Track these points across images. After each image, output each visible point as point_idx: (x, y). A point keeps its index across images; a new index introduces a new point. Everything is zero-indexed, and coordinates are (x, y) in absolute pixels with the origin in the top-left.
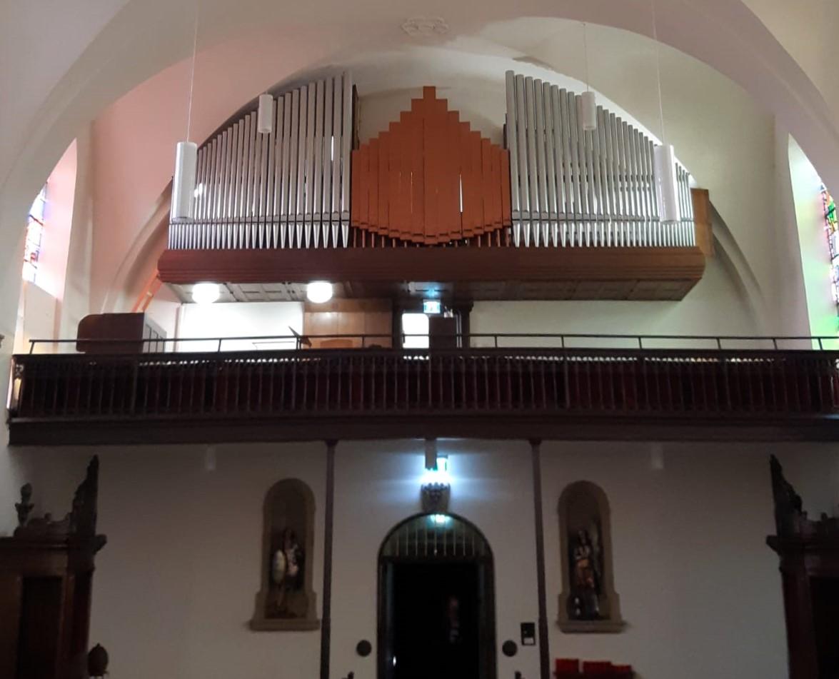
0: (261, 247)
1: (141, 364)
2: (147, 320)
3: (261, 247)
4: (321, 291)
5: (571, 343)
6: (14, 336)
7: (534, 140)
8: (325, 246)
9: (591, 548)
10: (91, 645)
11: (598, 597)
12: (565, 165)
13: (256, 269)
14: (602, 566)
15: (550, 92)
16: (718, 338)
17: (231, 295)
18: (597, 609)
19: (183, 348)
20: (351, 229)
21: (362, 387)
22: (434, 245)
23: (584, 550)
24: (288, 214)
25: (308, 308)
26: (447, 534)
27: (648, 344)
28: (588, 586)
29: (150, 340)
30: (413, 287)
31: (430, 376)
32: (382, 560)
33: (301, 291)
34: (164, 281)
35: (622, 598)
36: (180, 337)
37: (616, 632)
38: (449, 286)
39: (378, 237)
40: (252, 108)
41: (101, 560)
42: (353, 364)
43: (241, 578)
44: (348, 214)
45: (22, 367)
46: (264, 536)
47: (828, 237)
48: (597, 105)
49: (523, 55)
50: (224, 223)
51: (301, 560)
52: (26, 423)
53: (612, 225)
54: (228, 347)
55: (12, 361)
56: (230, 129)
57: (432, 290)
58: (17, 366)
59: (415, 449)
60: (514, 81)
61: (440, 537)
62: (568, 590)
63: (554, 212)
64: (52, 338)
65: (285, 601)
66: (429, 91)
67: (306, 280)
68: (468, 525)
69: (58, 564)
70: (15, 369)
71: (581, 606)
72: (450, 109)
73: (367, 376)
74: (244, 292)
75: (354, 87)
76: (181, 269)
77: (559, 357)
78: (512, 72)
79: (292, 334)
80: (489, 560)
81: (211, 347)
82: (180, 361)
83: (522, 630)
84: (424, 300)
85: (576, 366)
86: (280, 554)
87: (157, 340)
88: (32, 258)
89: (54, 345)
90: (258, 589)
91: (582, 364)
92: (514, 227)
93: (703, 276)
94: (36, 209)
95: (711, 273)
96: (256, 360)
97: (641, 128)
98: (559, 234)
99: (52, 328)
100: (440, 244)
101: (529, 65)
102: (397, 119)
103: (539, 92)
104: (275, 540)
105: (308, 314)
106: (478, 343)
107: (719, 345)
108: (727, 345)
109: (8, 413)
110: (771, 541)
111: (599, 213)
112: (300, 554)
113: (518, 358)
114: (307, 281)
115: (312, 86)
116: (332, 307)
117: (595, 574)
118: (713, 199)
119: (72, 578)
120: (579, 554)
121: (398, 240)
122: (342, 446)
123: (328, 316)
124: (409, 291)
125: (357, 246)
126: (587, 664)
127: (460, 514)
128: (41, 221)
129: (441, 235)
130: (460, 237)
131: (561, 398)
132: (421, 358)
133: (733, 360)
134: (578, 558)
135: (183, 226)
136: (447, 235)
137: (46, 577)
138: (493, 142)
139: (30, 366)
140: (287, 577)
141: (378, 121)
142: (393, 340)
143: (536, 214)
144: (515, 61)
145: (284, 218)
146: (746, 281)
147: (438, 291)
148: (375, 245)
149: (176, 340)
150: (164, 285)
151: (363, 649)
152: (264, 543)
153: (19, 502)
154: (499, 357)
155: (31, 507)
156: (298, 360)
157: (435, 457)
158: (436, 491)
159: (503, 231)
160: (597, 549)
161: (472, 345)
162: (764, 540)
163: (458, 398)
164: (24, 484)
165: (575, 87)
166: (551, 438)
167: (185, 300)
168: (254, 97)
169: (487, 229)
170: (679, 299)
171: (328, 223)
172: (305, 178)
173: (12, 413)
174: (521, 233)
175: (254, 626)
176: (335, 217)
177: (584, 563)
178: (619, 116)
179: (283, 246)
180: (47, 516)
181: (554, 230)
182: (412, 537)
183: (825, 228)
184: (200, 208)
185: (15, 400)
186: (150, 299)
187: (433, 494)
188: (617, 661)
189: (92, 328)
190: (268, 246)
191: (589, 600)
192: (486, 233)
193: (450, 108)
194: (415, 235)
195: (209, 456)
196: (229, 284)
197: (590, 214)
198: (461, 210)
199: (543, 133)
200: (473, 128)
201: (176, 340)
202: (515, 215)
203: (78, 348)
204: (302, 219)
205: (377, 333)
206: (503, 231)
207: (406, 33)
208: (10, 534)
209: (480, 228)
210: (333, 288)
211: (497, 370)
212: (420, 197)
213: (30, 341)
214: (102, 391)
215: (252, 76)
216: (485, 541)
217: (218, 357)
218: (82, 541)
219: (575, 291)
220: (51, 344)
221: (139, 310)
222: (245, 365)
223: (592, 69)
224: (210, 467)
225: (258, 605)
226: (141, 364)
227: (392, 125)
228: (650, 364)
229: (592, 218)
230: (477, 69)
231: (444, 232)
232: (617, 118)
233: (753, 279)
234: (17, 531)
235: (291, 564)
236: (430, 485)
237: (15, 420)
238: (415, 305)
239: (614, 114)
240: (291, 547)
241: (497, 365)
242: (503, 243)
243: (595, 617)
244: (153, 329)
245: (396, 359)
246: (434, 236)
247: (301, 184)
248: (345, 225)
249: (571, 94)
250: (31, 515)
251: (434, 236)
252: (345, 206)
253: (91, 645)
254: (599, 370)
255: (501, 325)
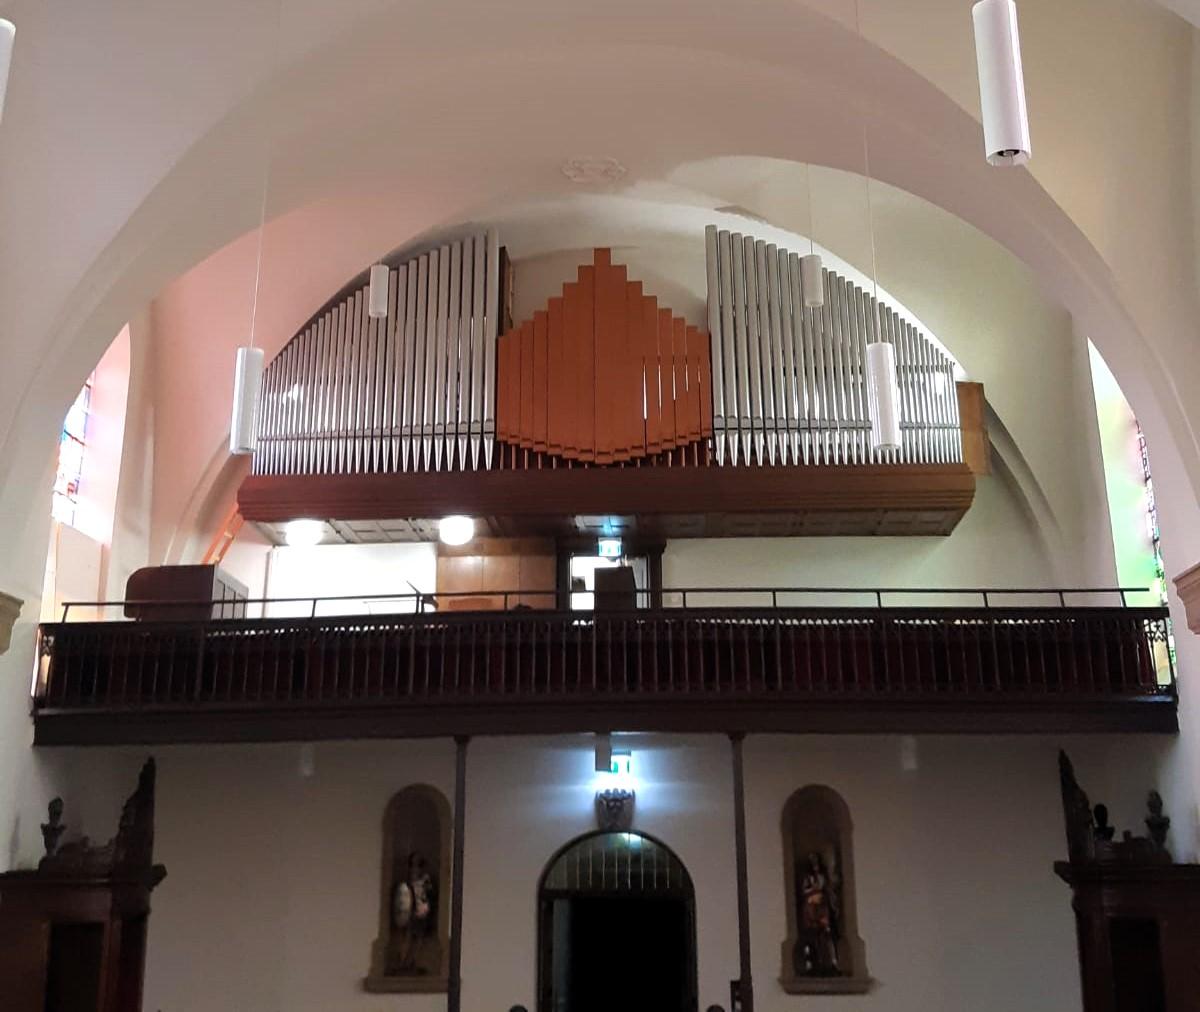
0: (462, 468)
2: (217, 575)
3: (462, 468)
4: (458, 529)
5: (785, 601)
9: (827, 878)
11: (835, 945)
12: (786, 353)
13: (372, 498)
14: (841, 904)
15: (764, 254)
16: (984, 592)
17: (338, 535)
19: (275, 612)
22: (608, 466)
23: (816, 880)
24: (483, 420)
25: (443, 551)
26: (637, 857)
27: (890, 601)
28: (822, 928)
29: (223, 602)
30: (582, 522)
31: (995, 647)
36: (269, 597)
37: (863, 992)
38: (630, 520)
39: (533, 455)
40: (361, 283)
41: (160, 900)
43: (352, 924)
45: (52, 639)
46: (384, 861)
47: (1141, 449)
48: (823, 266)
49: (729, 204)
50: (342, 437)
51: (432, 897)
52: (58, 716)
53: (830, 436)
54: (325, 610)
56: (342, 305)
57: (610, 524)
59: (581, 745)
61: (623, 861)
63: (770, 418)
64: (95, 600)
65: (416, 948)
66: (603, 253)
67: (438, 515)
68: (660, 844)
69: (98, 905)
70: (42, 641)
71: (812, 957)
72: (630, 278)
73: (678, 645)
74: (356, 532)
75: (503, 250)
76: (268, 499)
78: (714, 227)
81: (302, 611)
83: (732, 987)
84: (600, 539)
85: (792, 632)
86: (405, 888)
87: (234, 602)
89: (98, 610)
90: (375, 935)
91: (829, 629)
92: (717, 438)
93: (973, 504)
94: (74, 420)
95: (985, 494)
96: (738, 620)
98: (765, 448)
100: (616, 464)
102: (559, 293)
103: (750, 254)
105: (443, 559)
106: (673, 601)
107: (1063, 602)
108: (995, 601)
109: (32, 701)
110: (1060, 869)
114: (439, 515)
115: (445, 250)
116: (476, 549)
119: (118, 923)
120: (809, 887)
121: (559, 458)
122: (477, 743)
123: (470, 562)
124: (576, 527)
125: (517, 466)
128: (81, 440)
129: (617, 451)
130: (643, 454)
131: (771, 677)
132: (583, 623)
134: (808, 891)
137: (79, 925)
139: (63, 638)
140: (414, 920)
141: (535, 295)
142: (557, 599)
143: (746, 420)
144: (717, 212)
145: (406, 431)
147: (617, 526)
149: (264, 601)
150: (248, 525)
153: (46, 821)
156: (343, 629)
157: (609, 753)
158: (615, 800)
159: (701, 446)
160: (834, 878)
161: (665, 605)
163: (632, 679)
164: (53, 798)
165: (795, 244)
167: (276, 543)
169: (681, 442)
170: (947, 534)
172: (459, 374)
173: (38, 702)
174: (725, 448)
175: (370, 986)
177: (816, 898)
178: (858, 285)
181: (759, 441)
182: (584, 864)
183: (1138, 436)
185: (42, 684)
186: (228, 543)
189: (146, 586)
191: (822, 948)
192: (679, 448)
193: (631, 277)
194: (583, 451)
195: (305, 758)
196: (333, 521)
197: (864, 421)
200: (661, 304)
201: (264, 601)
202: (718, 423)
206: (702, 444)
207: (569, 178)
208: (35, 864)
210: (476, 524)
212: (589, 402)
213: (63, 604)
215: (355, 240)
217: (312, 623)
218: (133, 872)
220: (95, 608)
221: (211, 562)
222: (273, 635)
224: (307, 770)
228: (708, 627)
229: (832, 426)
230: (668, 221)
231: (622, 447)
233: (1045, 502)
234: (43, 862)
235: (419, 901)
236: (607, 792)
238: (588, 544)
239: (852, 283)
240: (420, 877)
242: (702, 461)
244: (226, 582)
246: (608, 453)
248: (489, 439)
249: (782, 251)
250: (61, 841)
251: (608, 453)
252: (488, 413)
254: (746, 638)
255: (710, 575)
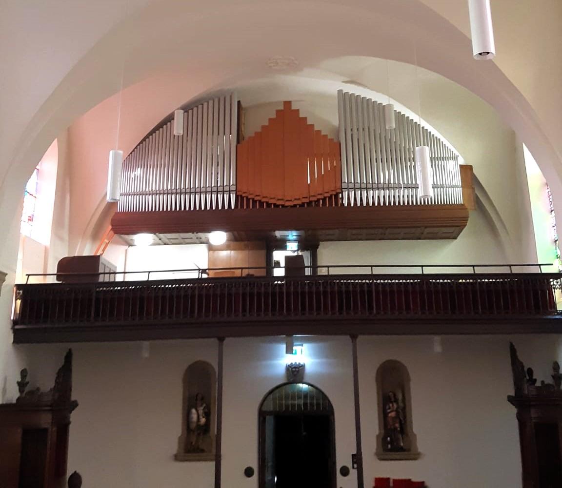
1: (98, 289)
2: (102, 260)
4: (219, 237)
5: (377, 271)
6: (15, 272)
7: (373, 136)
8: (220, 208)
9: (397, 403)
10: (69, 473)
11: (402, 436)
14: (405, 417)
16: (473, 266)
18: (402, 444)
19: (129, 278)
20: (237, 197)
21: (160, 308)
22: (291, 206)
23: (393, 405)
25: (211, 248)
26: (306, 395)
27: (428, 271)
28: (396, 428)
29: (104, 273)
30: (278, 234)
32: (262, 415)
33: (206, 238)
34: (115, 233)
35: (418, 437)
36: (126, 271)
37: (415, 459)
39: (254, 202)
40: (170, 119)
41: (75, 417)
42: (257, 286)
44: (235, 186)
45: (21, 292)
46: (184, 399)
49: (348, 79)
52: (24, 329)
54: (154, 277)
55: (15, 288)
57: (292, 235)
58: (18, 291)
59: (280, 341)
60: (344, 98)
62: (383, 431)
66: (288, 104)
69: (45, 420)
70: (16, 293)
71: (391, 442)
75: (239, 102)
76: (126, 224)
77: (369, 280)
79: (198, 268)
80: (332, 412)
81: (143, 278)
82: (115, 287)
84: (287, 242)
86: (194, 411)
87: (110, 273)
88: (29, 220)
92: (344, 193)
94: (31, 186)
96: (172, 285)
97: (424, 124)
99: (42, 267)
100: (295, 206)
101: (353, 86)
103: (360, 104)
104: (190, 402)
109: (12, 323)
110: (511, 399)
111: (394, 183)
112: (206, 410)
113: (342, 281)
114: (209, 231)
115: (211, 103)
117: (401, 421)
118: (475, 171)
119: (55, 429)
120: (390, 408)
121: (267, 203)
123: (225, 254)
124: (276, 236)
125: (241, 207)
126: (395, 481)
127: (312, 383)
128: (34, 195)
133: (461, 281)
134: (389, 411)
135: (178, 196)
136: (299, 199)
138: (329, 137)
139: (27, 292)
140: (198, 426)
141: (255, 124)
143: (344, 184)
144: (344, 83)
146: (498, 225)
148: (253, 207)
150: (116, 236)
151: (249, 472)
152: (184, 403)
153: (20, 380)
154: (330, 281)
155: (28, 383)
159: (336, 196)
160: (401, 404)
161: (319, 274)
162: (506, 398)
163: (303, 309)
165: (382, 99)
166: (364, 334)
168: (170, 112)
170: (455, 238)
171: (194, 194)
172: (218, 163)
173: (15, 322)
174: (347, 198)
175: (177, 458)
176: (227, 189)
177: (393, 414)
179: (197, 209)
180: (38, 389)
183: (548, 191)
184: (125, 185)
186: (107, 244)
187: (294, 369)
188: (415, 479)
189: (67, 266)
190: (183, 209)
191: (396, 439)
192: (325, 198)
196: (157, 234)
198: (309, 183)
199: (356, 130)
200: (316, 128)
202: (344, 186)
203: (58, 279)
204: (216, 190)
205: (258, 266)
206: (337, 195)
209: (321, 194)
211: (299, 290)
212: (282, 175)
213: (27, 275)
214: (72, 309)
215: (168, 98)
216: (329, 401)
217: (148, 283)
218: (62, 404)
219: (385, 234)
220: (43, 276)
223: (393, 90)
225: (179, 443)
226: (98, 289)
227: (263, 127)
230: (319, 88)
232: (415, 122)
234: (18, 399)
235: (201, 417)
236: (292, 363)
237: (17, 327)
238: (281, 245)
240: (201, 406)
241: (329, 287)
243: (402, 449)
245: (270, 284)
247: (209, 167)
250: (27, 389)
253: (69, 473)
255: (341, 259)
